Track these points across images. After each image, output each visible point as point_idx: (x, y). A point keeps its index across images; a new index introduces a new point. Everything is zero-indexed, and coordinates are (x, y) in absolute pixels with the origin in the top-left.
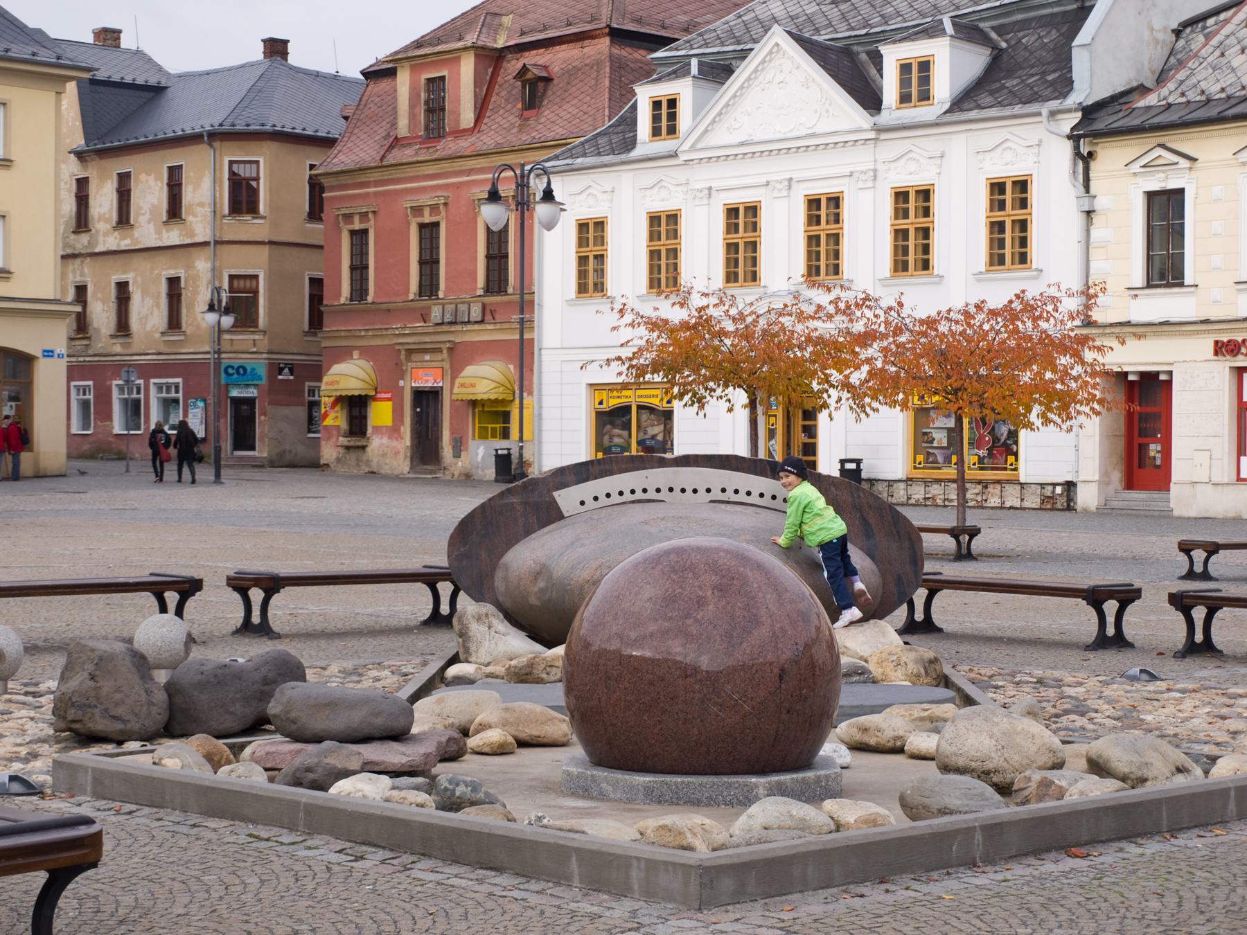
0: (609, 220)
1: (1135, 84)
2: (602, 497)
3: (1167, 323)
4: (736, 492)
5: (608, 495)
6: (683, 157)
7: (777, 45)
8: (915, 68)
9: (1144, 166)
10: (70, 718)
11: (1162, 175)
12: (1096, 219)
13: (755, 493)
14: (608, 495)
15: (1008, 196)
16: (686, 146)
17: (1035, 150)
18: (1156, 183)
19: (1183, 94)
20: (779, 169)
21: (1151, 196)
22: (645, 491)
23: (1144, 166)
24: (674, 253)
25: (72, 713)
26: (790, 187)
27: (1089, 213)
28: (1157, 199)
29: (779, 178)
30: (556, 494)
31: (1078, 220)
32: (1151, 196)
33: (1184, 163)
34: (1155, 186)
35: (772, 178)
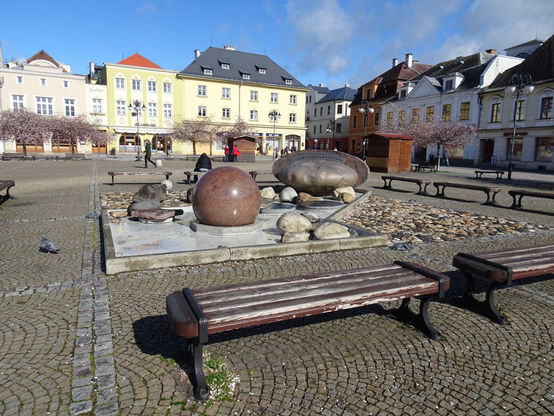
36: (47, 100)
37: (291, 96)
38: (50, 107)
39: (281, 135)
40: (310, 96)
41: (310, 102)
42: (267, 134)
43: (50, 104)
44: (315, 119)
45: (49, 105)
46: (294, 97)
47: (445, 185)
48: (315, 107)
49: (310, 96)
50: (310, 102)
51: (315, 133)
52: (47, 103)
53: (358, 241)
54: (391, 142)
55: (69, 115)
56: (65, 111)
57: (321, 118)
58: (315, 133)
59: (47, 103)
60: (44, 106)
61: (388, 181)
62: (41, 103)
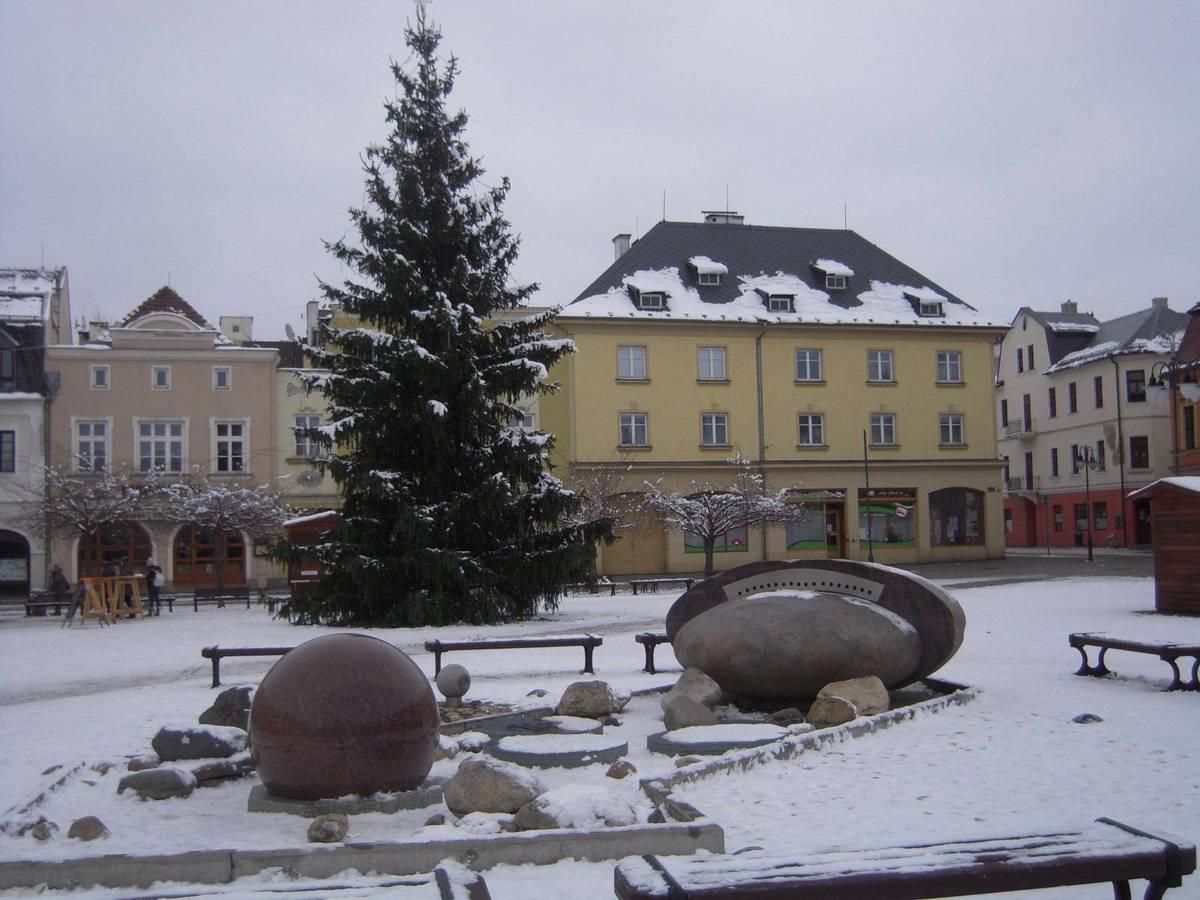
30: (724, 587)
36: (168, 430)
37: (941, 357)
38: (176, 447)
39: (912, 492)
40: (1031, 348)
41: (1032, 367)
42: (862, 493)
43: (176, 439)
44: (1054, 424)
45: (173, 444)
46: (954, 357)
47: (1106, 645)
48: (1047, 384)
49: (1031, 348)
50: (1032, 367)
51: (1056, 473)
52: (168, 438)
53: (558, 827)
54: (22, 563)
55: (226, 468)
56: (214, 453)
57: (1075, 419)
58: (1056, 473)
59: (168, 438)
60: (160, 446)
61: (1093, 652)
62: (153, 438)
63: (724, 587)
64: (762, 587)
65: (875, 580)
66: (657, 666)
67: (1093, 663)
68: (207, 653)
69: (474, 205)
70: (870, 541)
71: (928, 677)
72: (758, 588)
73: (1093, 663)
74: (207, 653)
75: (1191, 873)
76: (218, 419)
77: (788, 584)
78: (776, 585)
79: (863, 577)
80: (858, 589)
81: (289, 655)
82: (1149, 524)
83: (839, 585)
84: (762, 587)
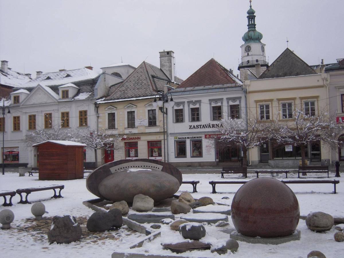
0: (70, 112)
1: (104, 96)
2: (148, 167)
3: (142, 133)
4: (147, 166)
5: (147, 166)
6: (21, 107)
7: (39, 87)
8: (65, 92)
9: (149, 105)
10: (52, 240)
11: (131, 109)
12: (99, 118)
13: (155, 167)
14: (152, 167)
15: (32, 118)
16: (21, 105)
17: (88, 106)
18: (110, 112)
19: (114, 97)
20: (40, 109)
21: (109, 114)
22: (126, 167)
23: (149, 105)
24: (19, 124)
25: (336, 238)
26: (42, 112)
27: (98, 117)
28: (110, 114)
29: (39, 110)
30: (110, 169)
31: (96, 118)
32: (109, 114)
33: (115, 109)
34: (129, 110)
35: (38, 110)
63: (110, 169)
64: (131, 167)
65: (160, 165)
66: (217, 190)
67: (57, 194)
68: (210, 183)
69: (37, 225)
70: (58, 117)
71: (174, 194)
72: (133, 167)
73: (57, 194)
74: (210, 183)
75: (44, 206)
76: (198, 242)
77: (133, 167)
78: (129, 167)
79: (156, 164)
80: (158, 168)
81: (246, 184)
82: (61, 120)
83: (154, 167)
84: (134, 166)
